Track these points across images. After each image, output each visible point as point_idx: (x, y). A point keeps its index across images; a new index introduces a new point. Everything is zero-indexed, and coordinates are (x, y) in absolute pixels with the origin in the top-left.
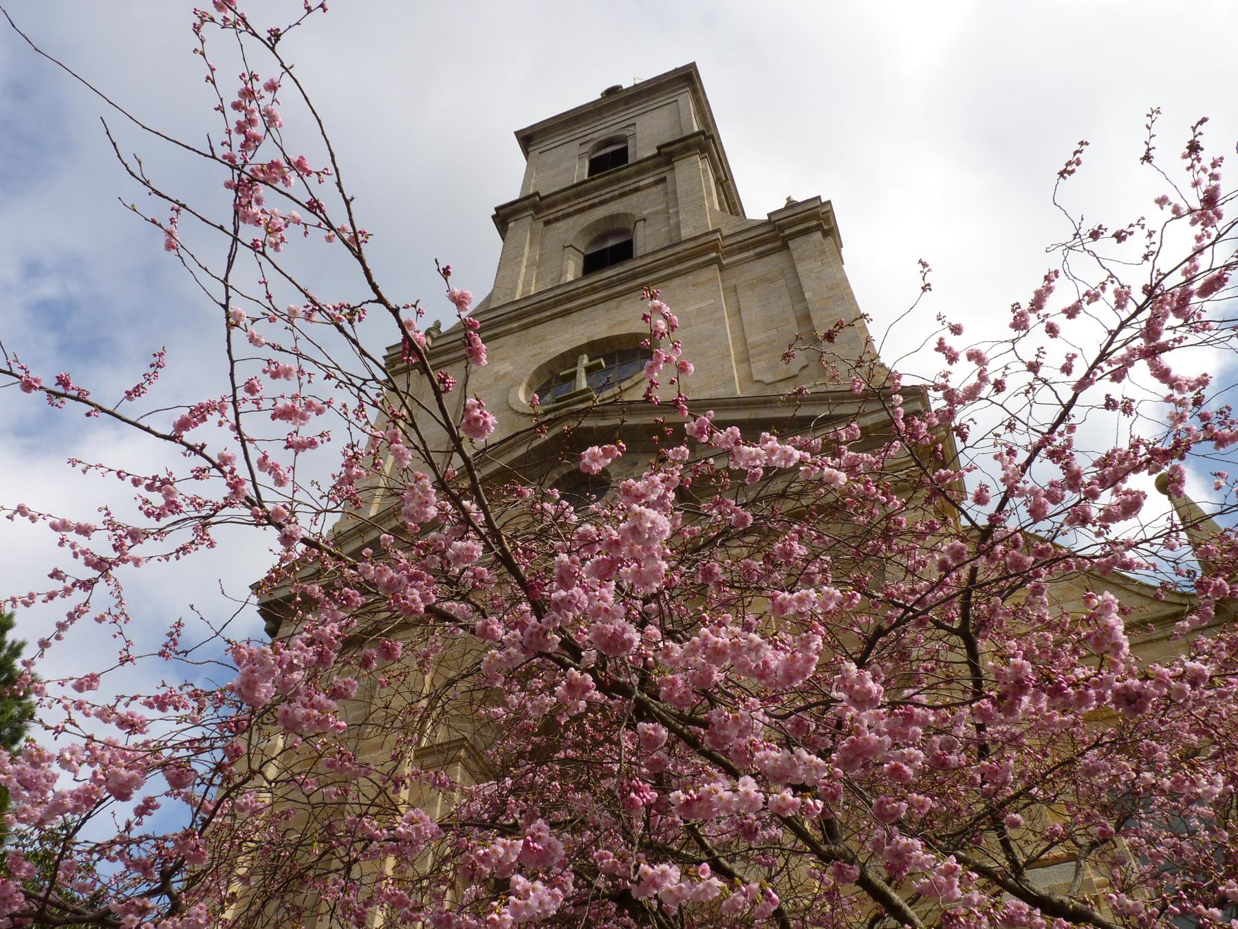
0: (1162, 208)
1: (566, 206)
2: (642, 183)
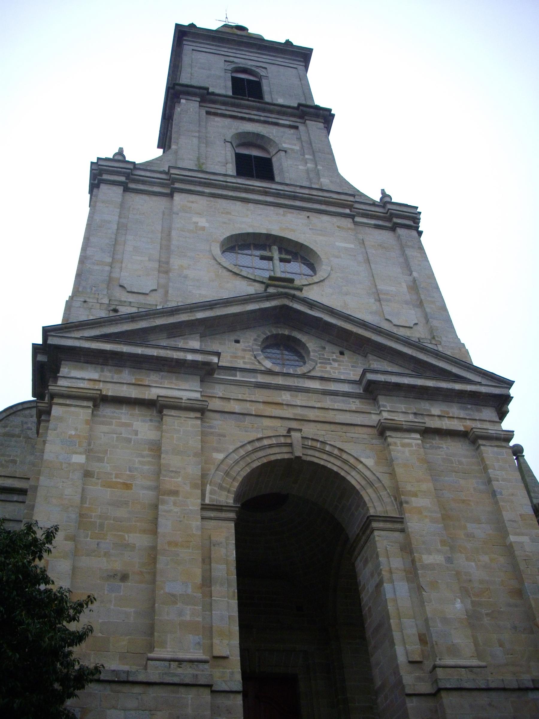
0: (383, 192)
1: (223, 108)
2: (281, 122)
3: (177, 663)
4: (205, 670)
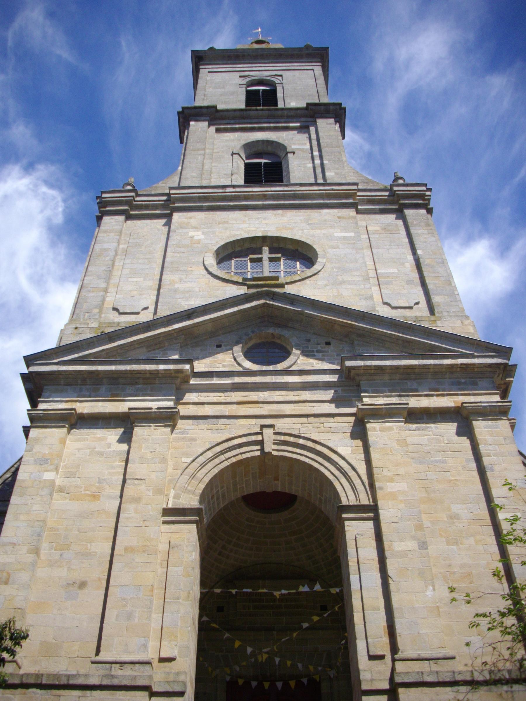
3: (118, 665)
4: (145, 671)
